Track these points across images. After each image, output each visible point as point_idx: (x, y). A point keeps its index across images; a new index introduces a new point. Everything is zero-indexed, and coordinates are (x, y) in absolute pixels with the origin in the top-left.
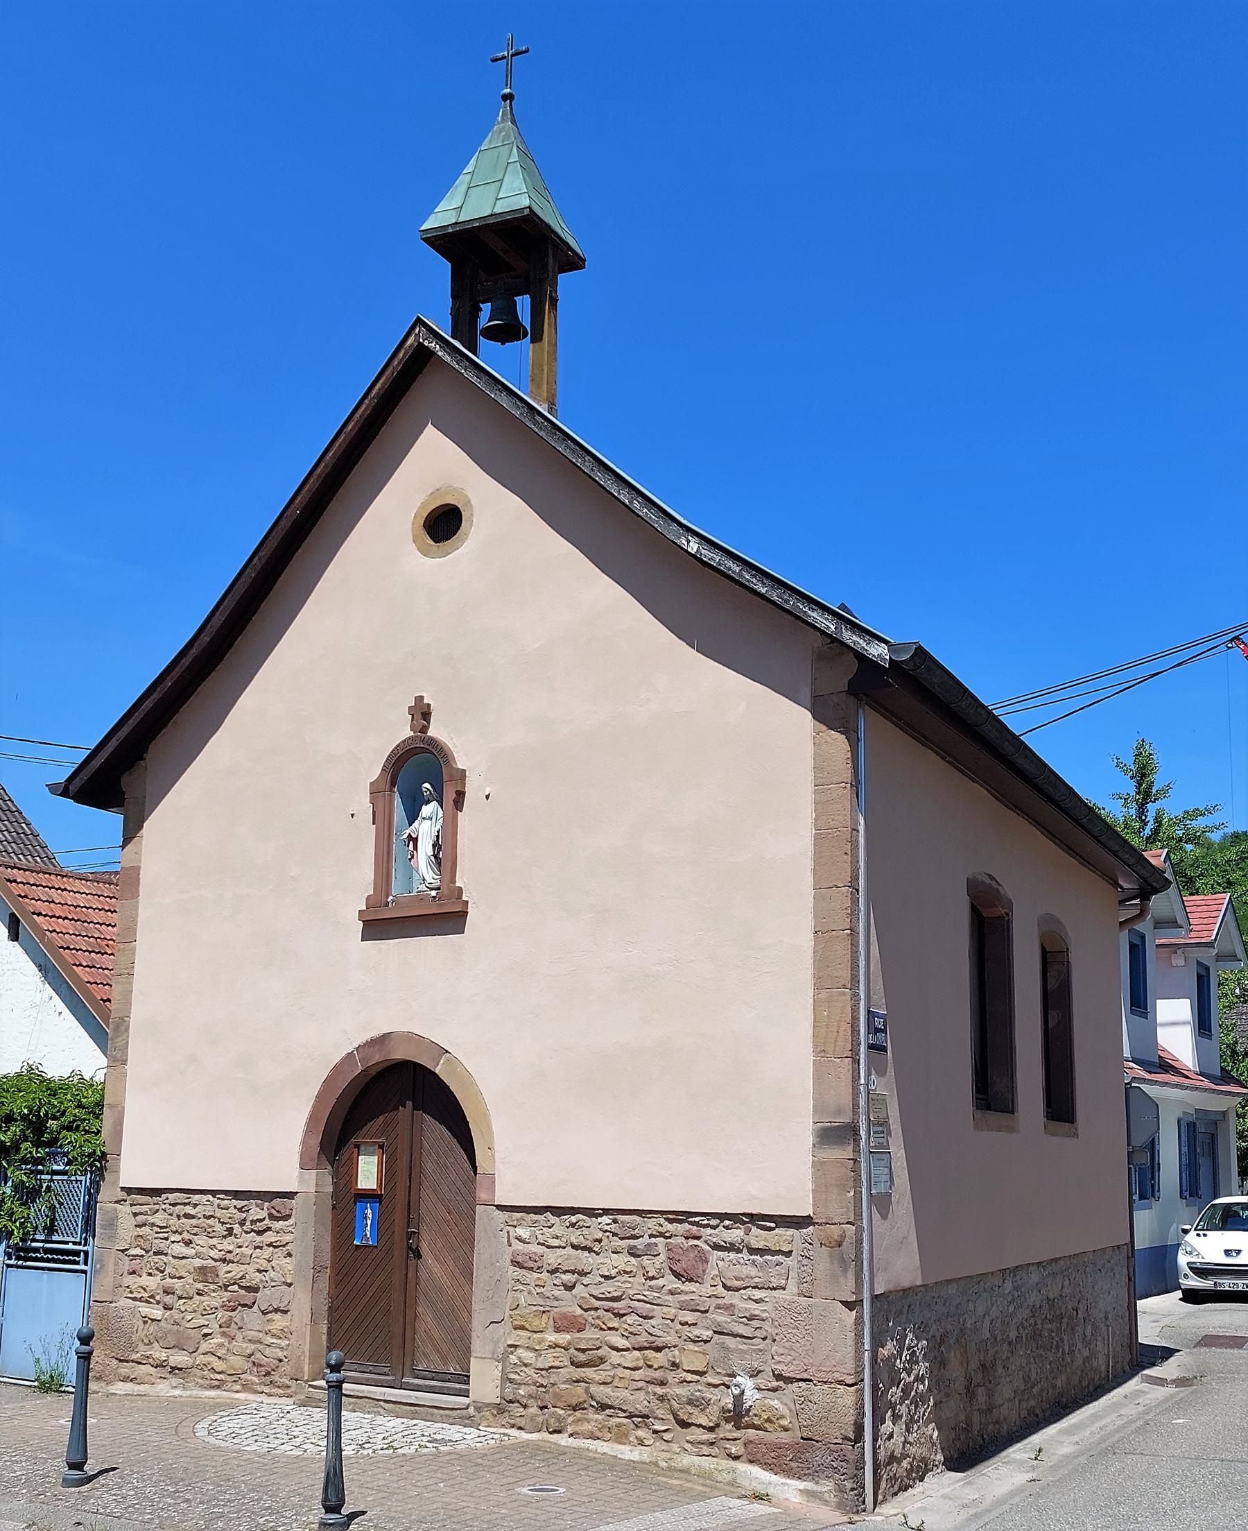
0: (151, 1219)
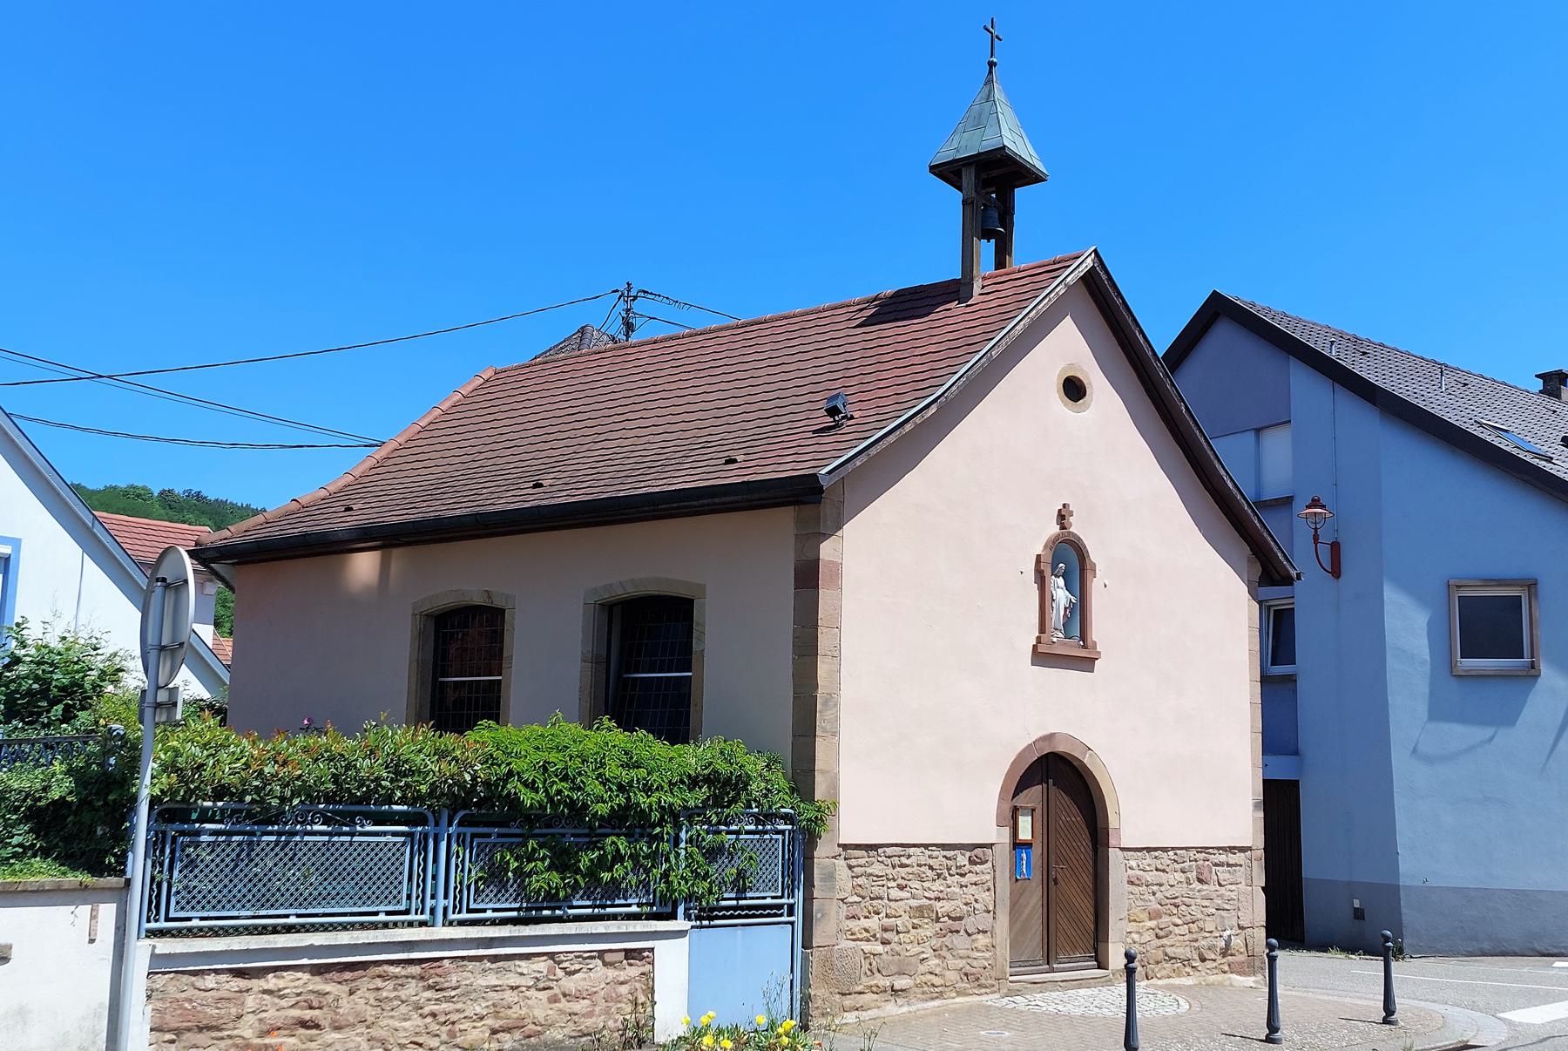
0: (869, 870)
